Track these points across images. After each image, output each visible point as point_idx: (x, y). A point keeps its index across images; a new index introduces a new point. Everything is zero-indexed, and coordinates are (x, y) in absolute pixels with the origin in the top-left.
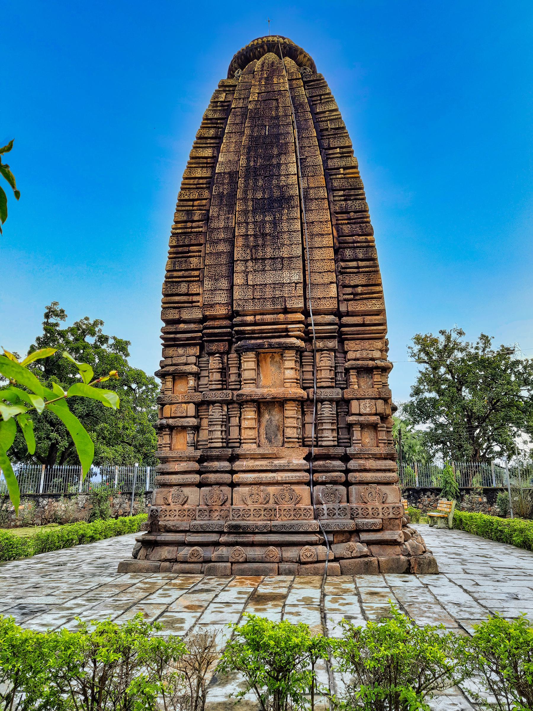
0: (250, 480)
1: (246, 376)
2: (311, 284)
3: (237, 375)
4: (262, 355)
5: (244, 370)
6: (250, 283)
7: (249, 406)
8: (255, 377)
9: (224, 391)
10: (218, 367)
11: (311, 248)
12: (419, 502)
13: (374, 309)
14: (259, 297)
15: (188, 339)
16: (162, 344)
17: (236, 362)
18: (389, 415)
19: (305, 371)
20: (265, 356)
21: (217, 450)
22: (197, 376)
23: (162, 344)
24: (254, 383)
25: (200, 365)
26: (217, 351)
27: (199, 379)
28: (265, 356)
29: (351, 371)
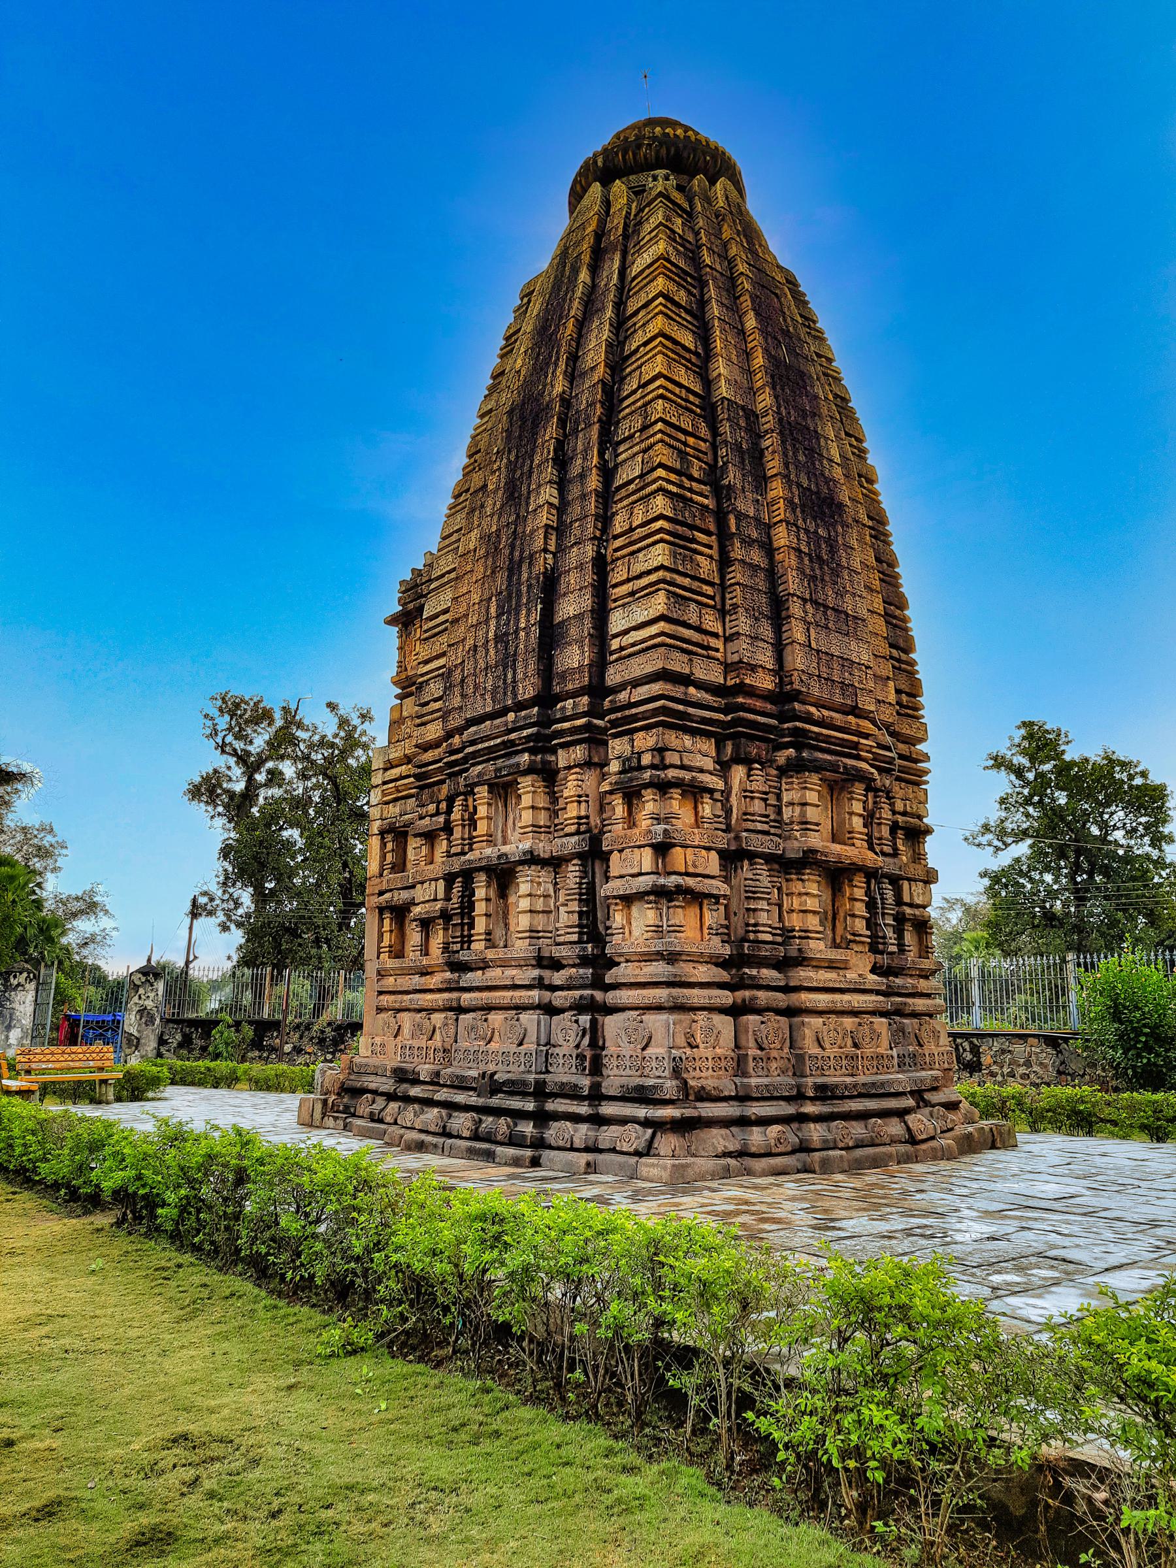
0: (821, 1006)
12: (341, 1050)
15: (704, 721)
18: (967, 910)
21: (768, 946)
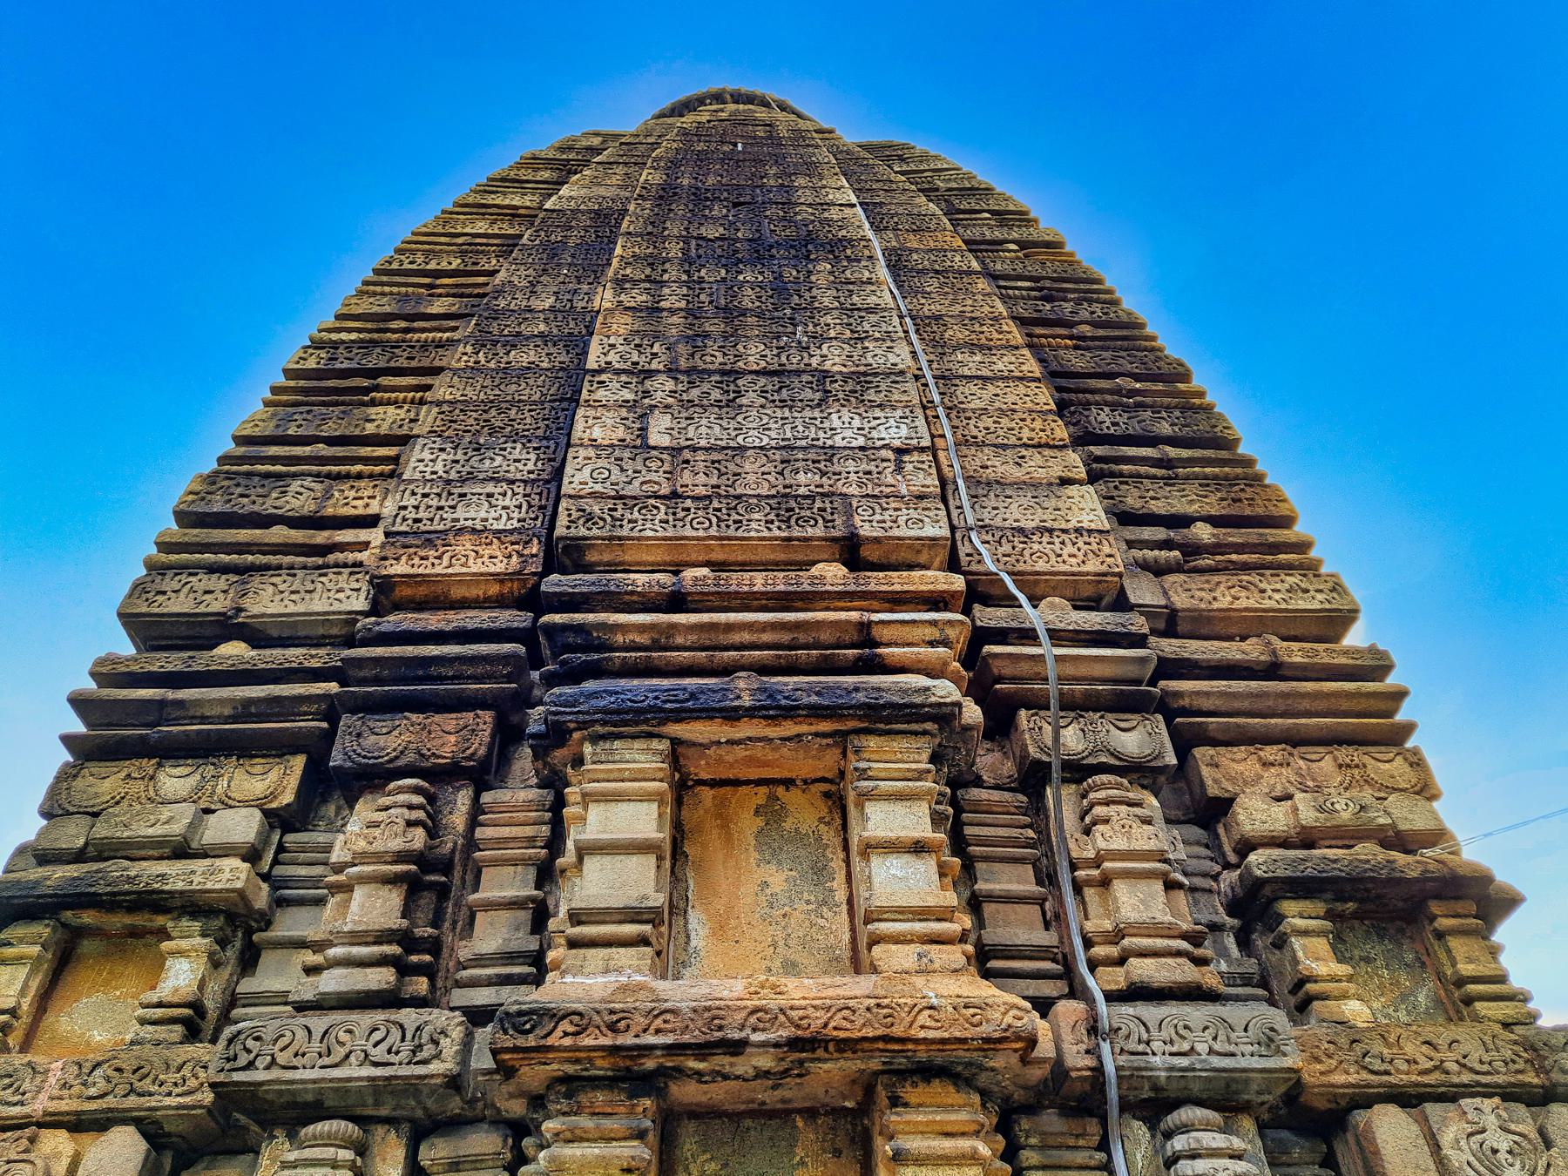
1: (593, 891)
2: (967, 479)
3: (525, 916)
4: (707, 794)
5: (583, 851)
6: (656, 437)
7: (585, 1122)
8: (658, 899)
9: (409, 1016)
10: (396, 844)
11: (943, 377)
13: (1302, 605)
14: (701, 491)
15: (246, 710)
16: (68, 740)
17: (529, 831)
19: (992, 898)
20: (722, 804)
22: (240, 931)
23: (68, 740)
24: (643, 941)
25: (279, 870)
26: (410, 757)
27: (249, 962)
28: (722, 804)
29: (1289, 907)
